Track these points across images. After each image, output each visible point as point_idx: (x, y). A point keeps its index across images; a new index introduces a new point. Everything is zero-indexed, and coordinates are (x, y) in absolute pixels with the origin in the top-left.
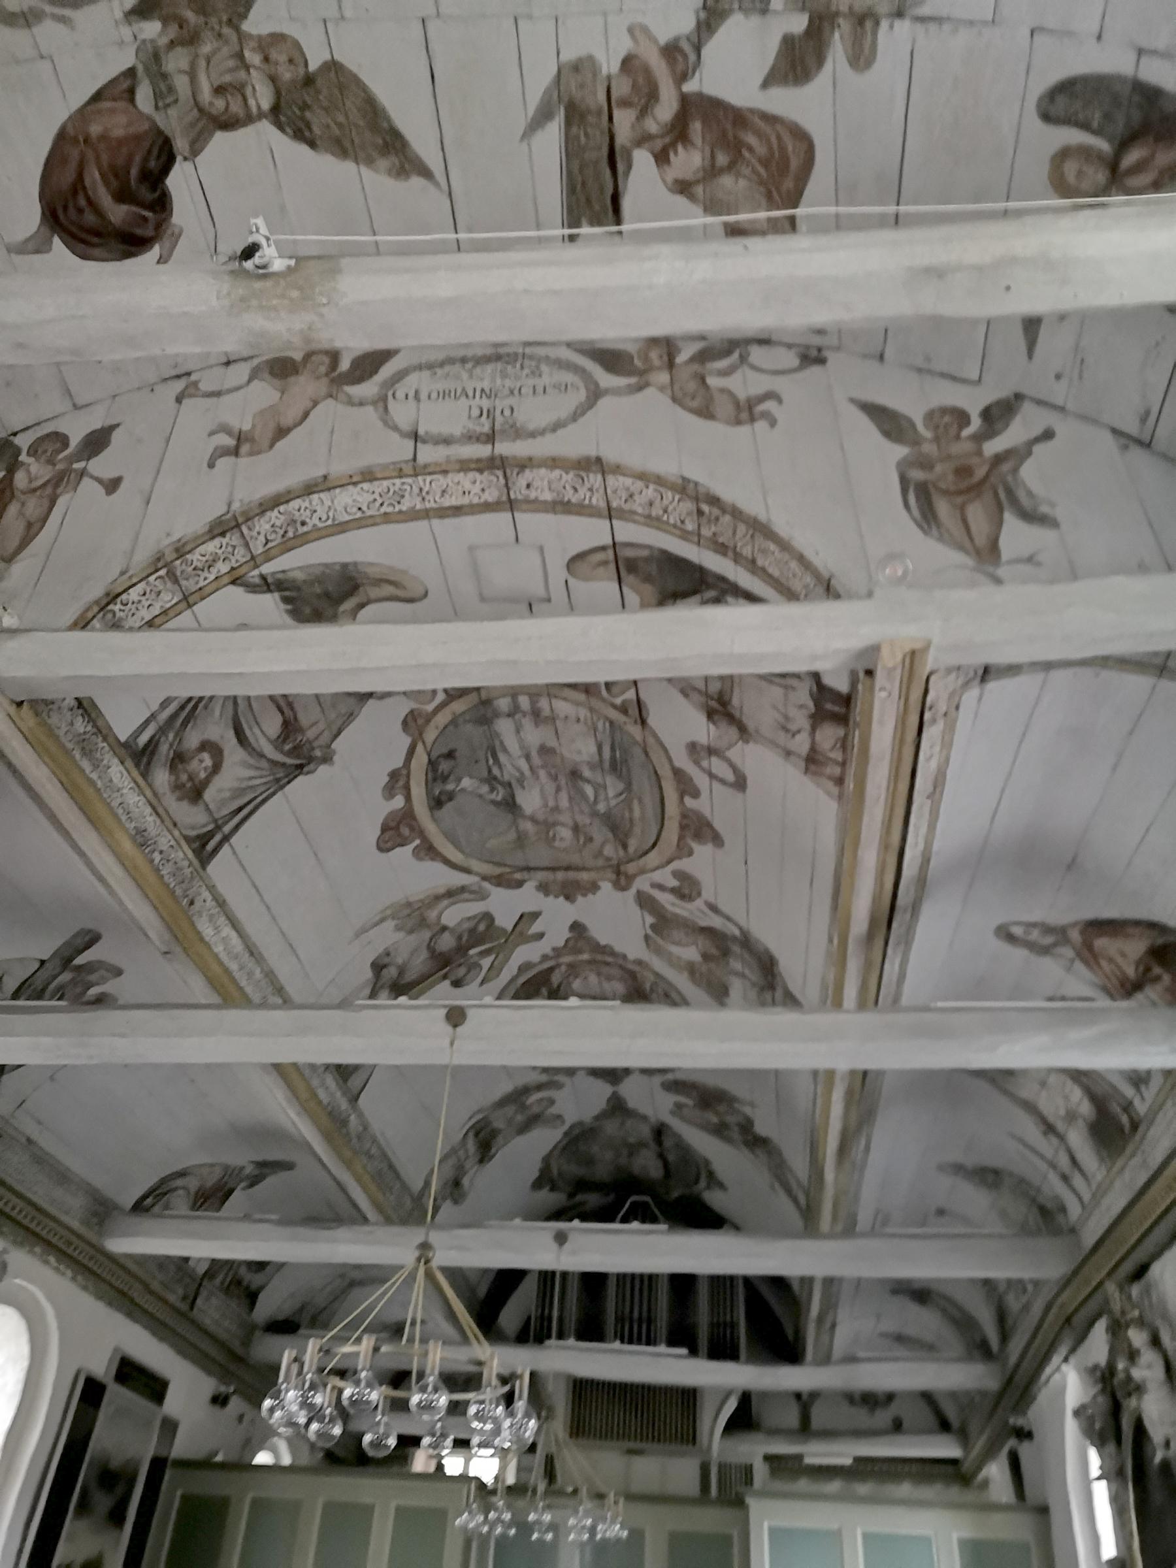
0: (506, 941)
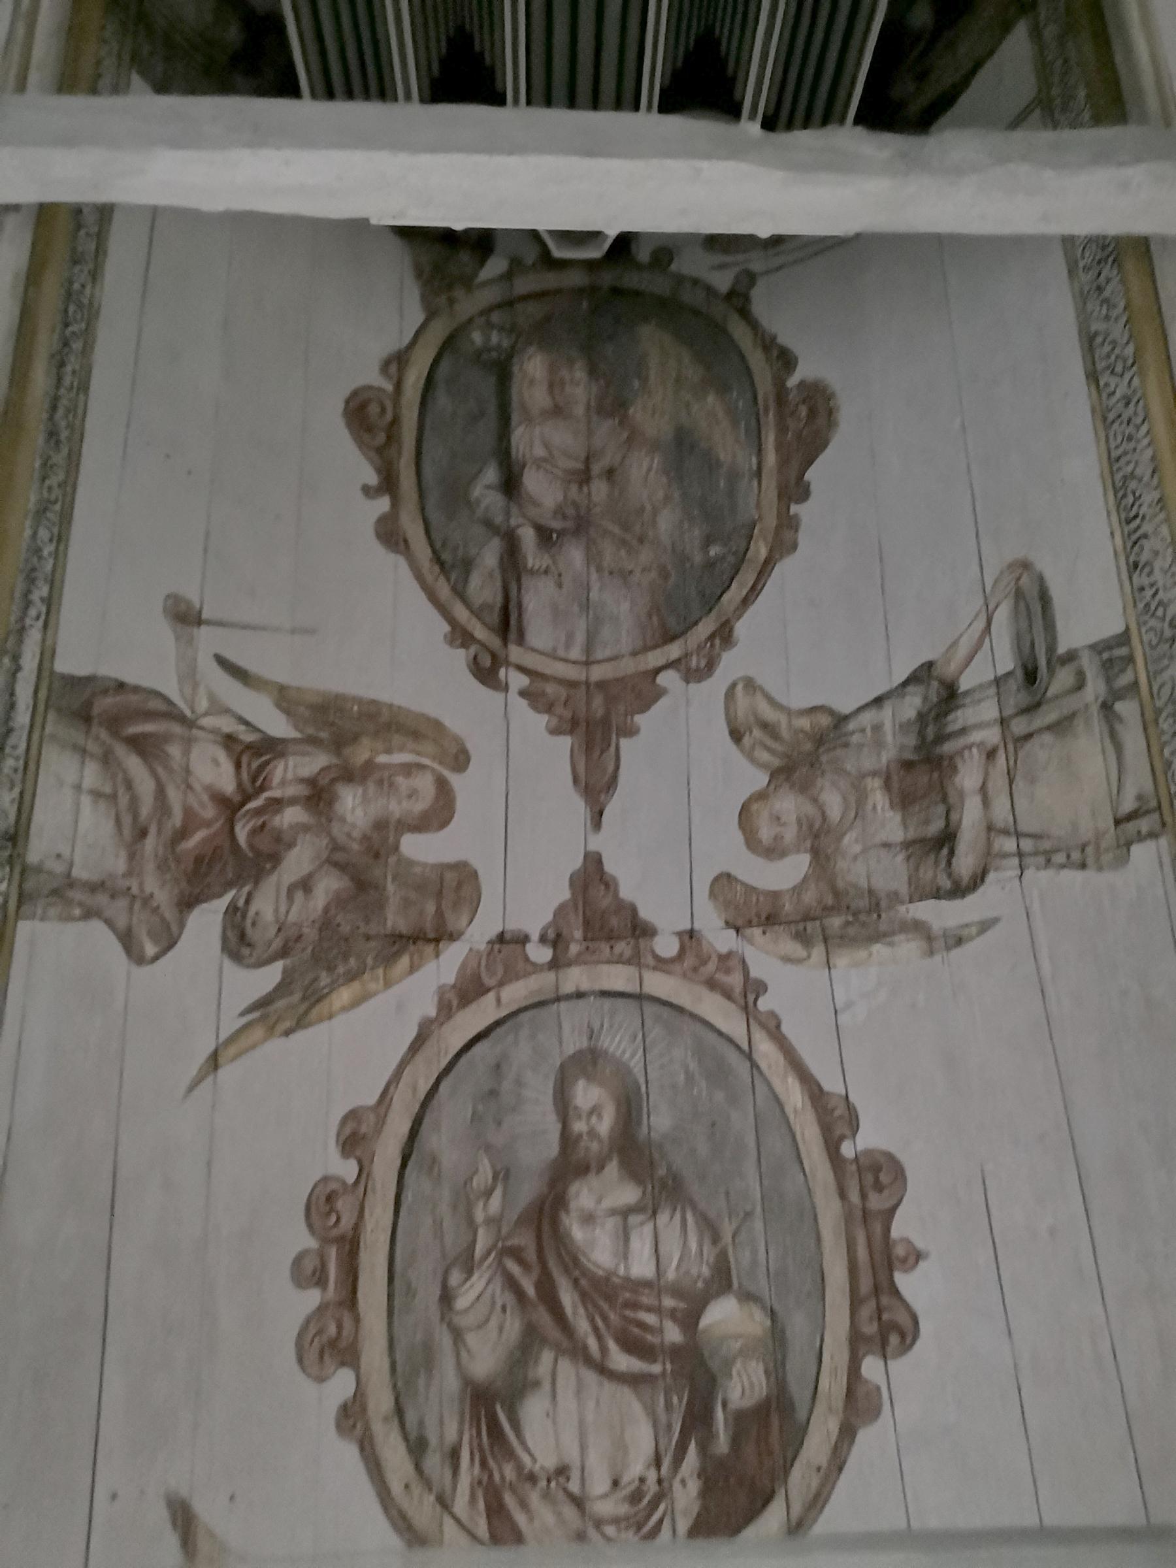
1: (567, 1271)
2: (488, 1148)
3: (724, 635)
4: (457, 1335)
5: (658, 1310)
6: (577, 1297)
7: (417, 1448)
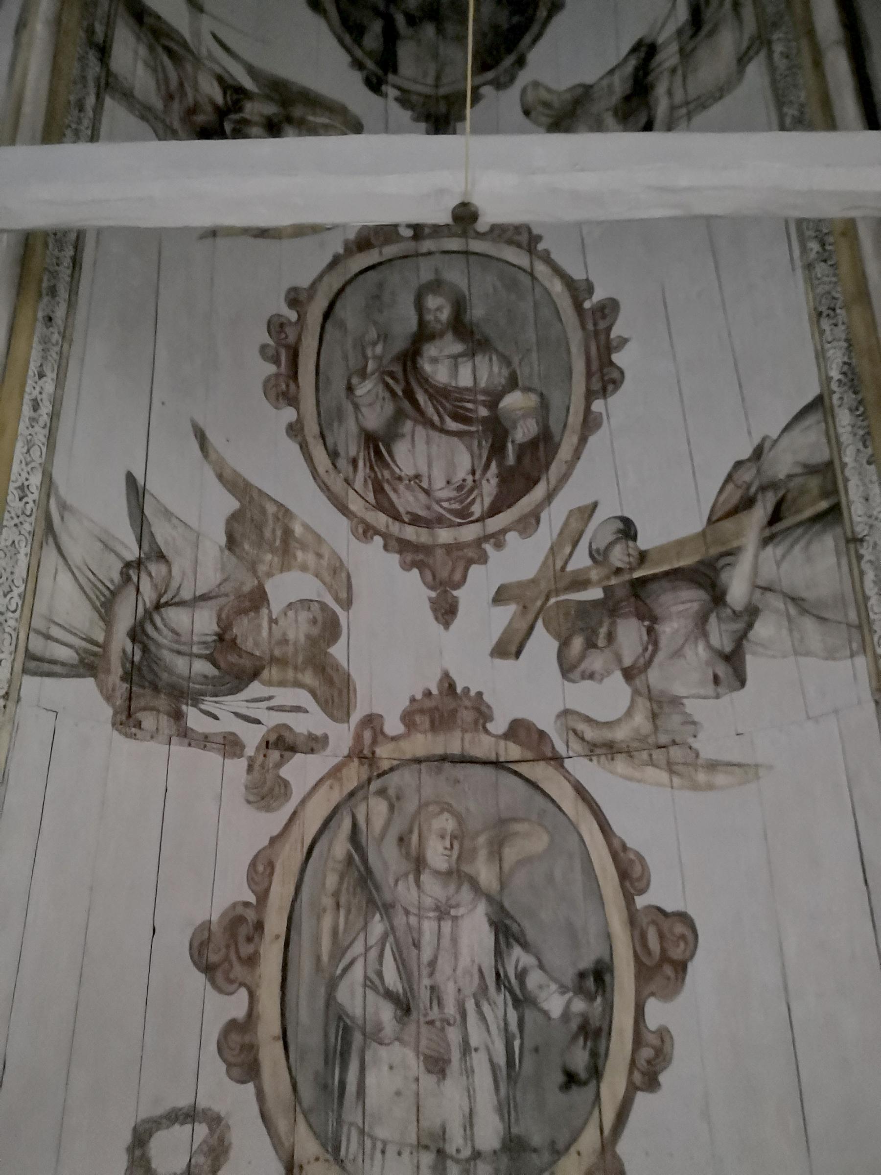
0: (547, 598)
1: (421, 386)
2: (375, 323)
3: (521, 62)
4: (356, 407)
5: (474, 402)
6: (427, 397)
7: (334, 455)
